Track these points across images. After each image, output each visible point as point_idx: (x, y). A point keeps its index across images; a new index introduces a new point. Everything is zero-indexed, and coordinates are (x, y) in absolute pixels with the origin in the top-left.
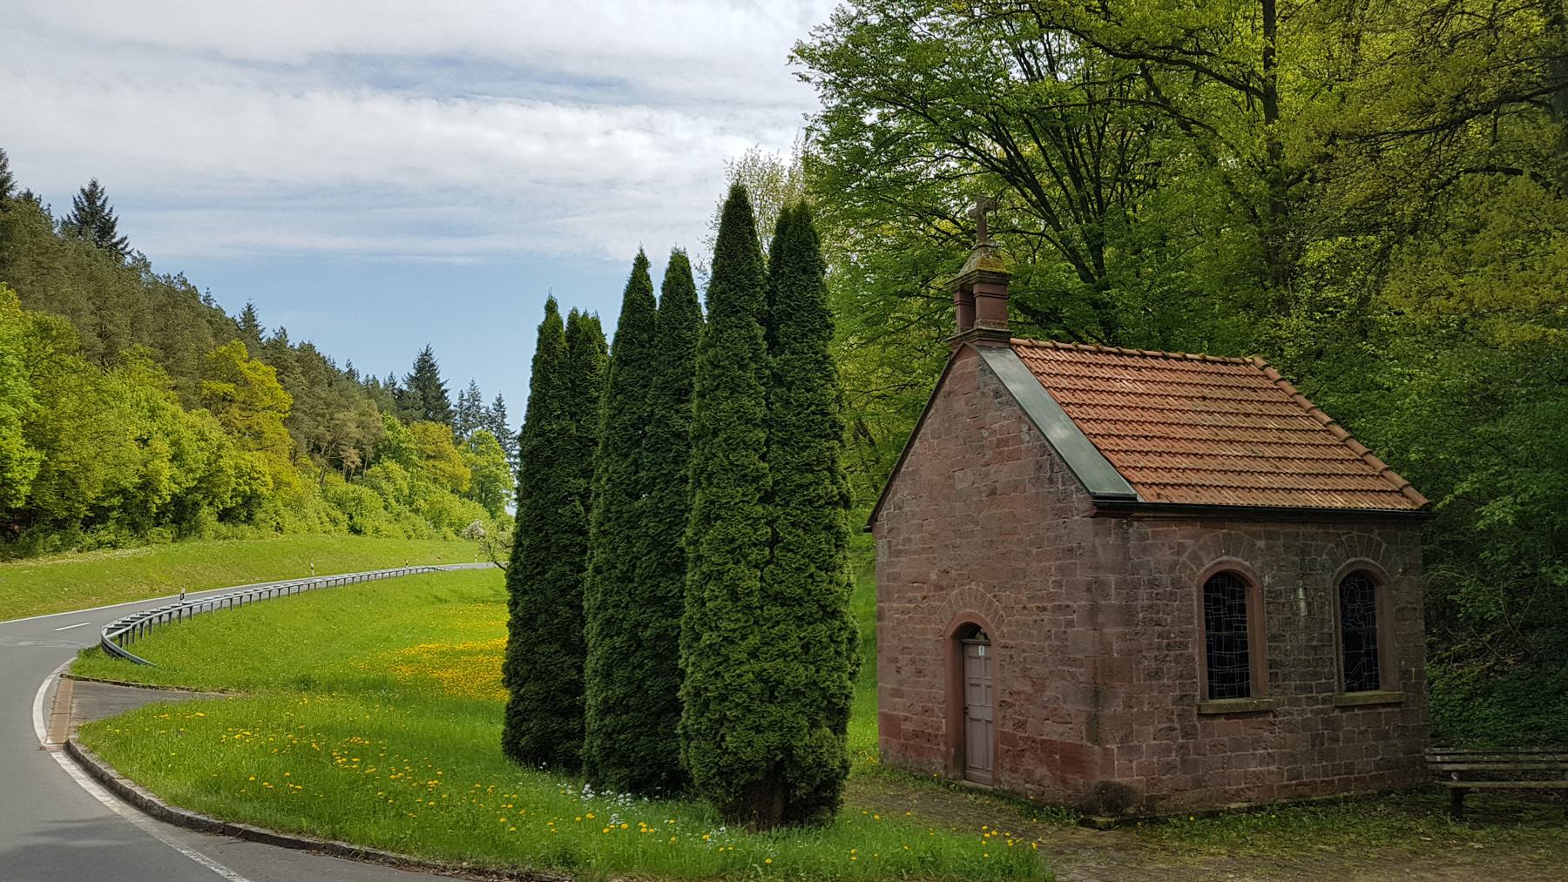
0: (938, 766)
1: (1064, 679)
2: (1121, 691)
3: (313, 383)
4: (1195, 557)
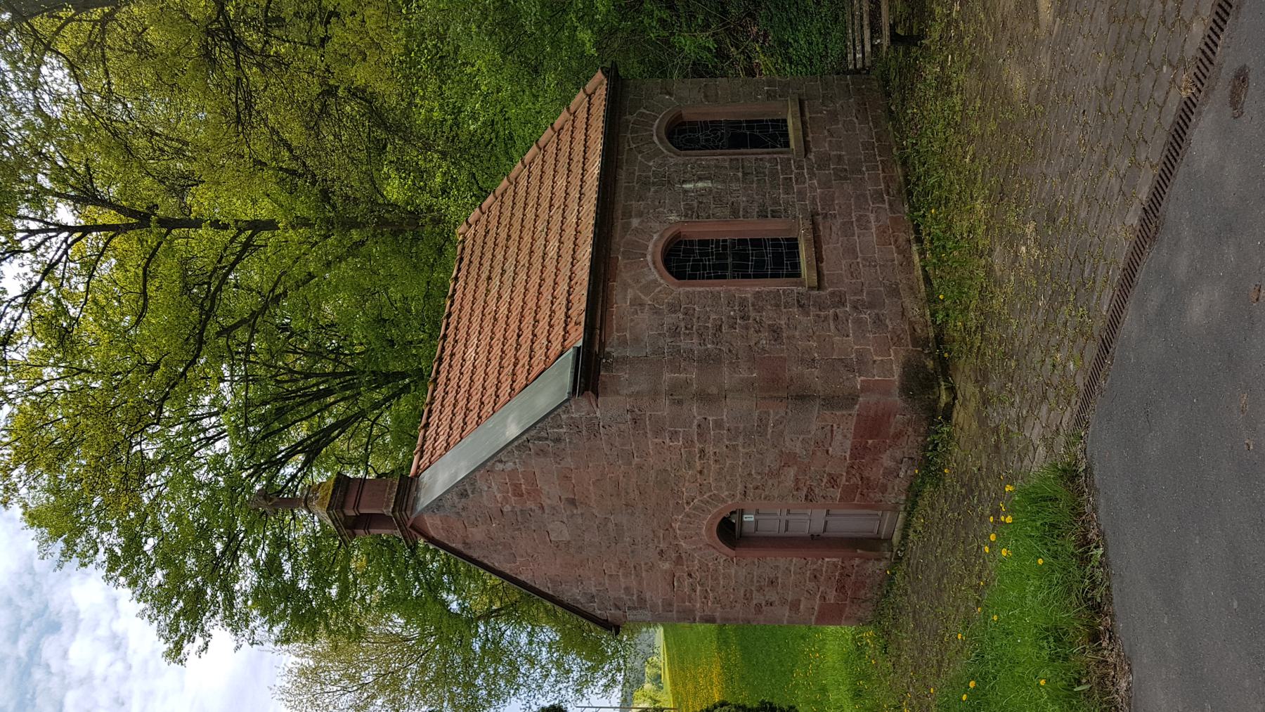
0: (876, 568)
2: (796, 370)
4: (647, 288)
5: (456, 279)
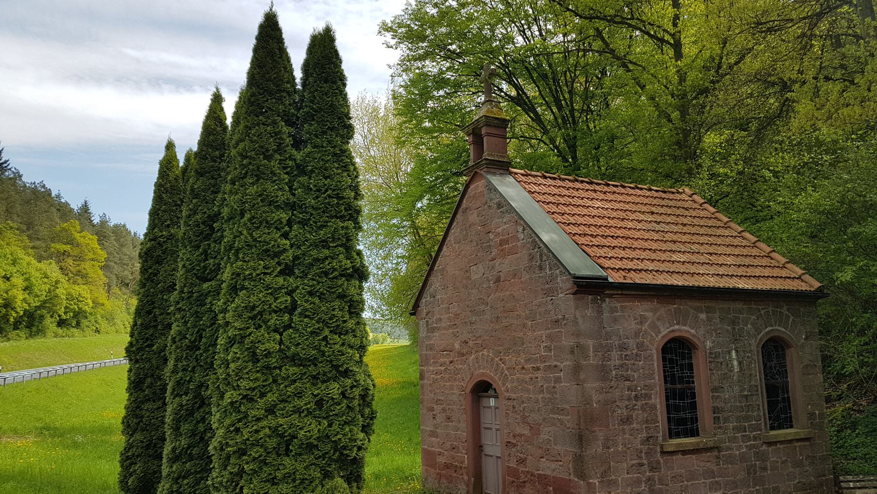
3: (122, 246)
4: (653, 327)
5: (650, 190)
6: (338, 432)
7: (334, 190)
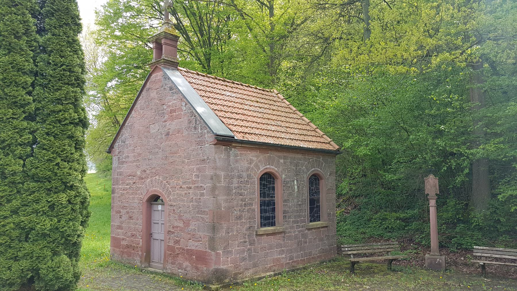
0: (137, 261)
1: (199, 220)
2: (225, 226)
4: (257, 166)
5: (256, 88)
6: (65, 226)
7: (67, 66)
